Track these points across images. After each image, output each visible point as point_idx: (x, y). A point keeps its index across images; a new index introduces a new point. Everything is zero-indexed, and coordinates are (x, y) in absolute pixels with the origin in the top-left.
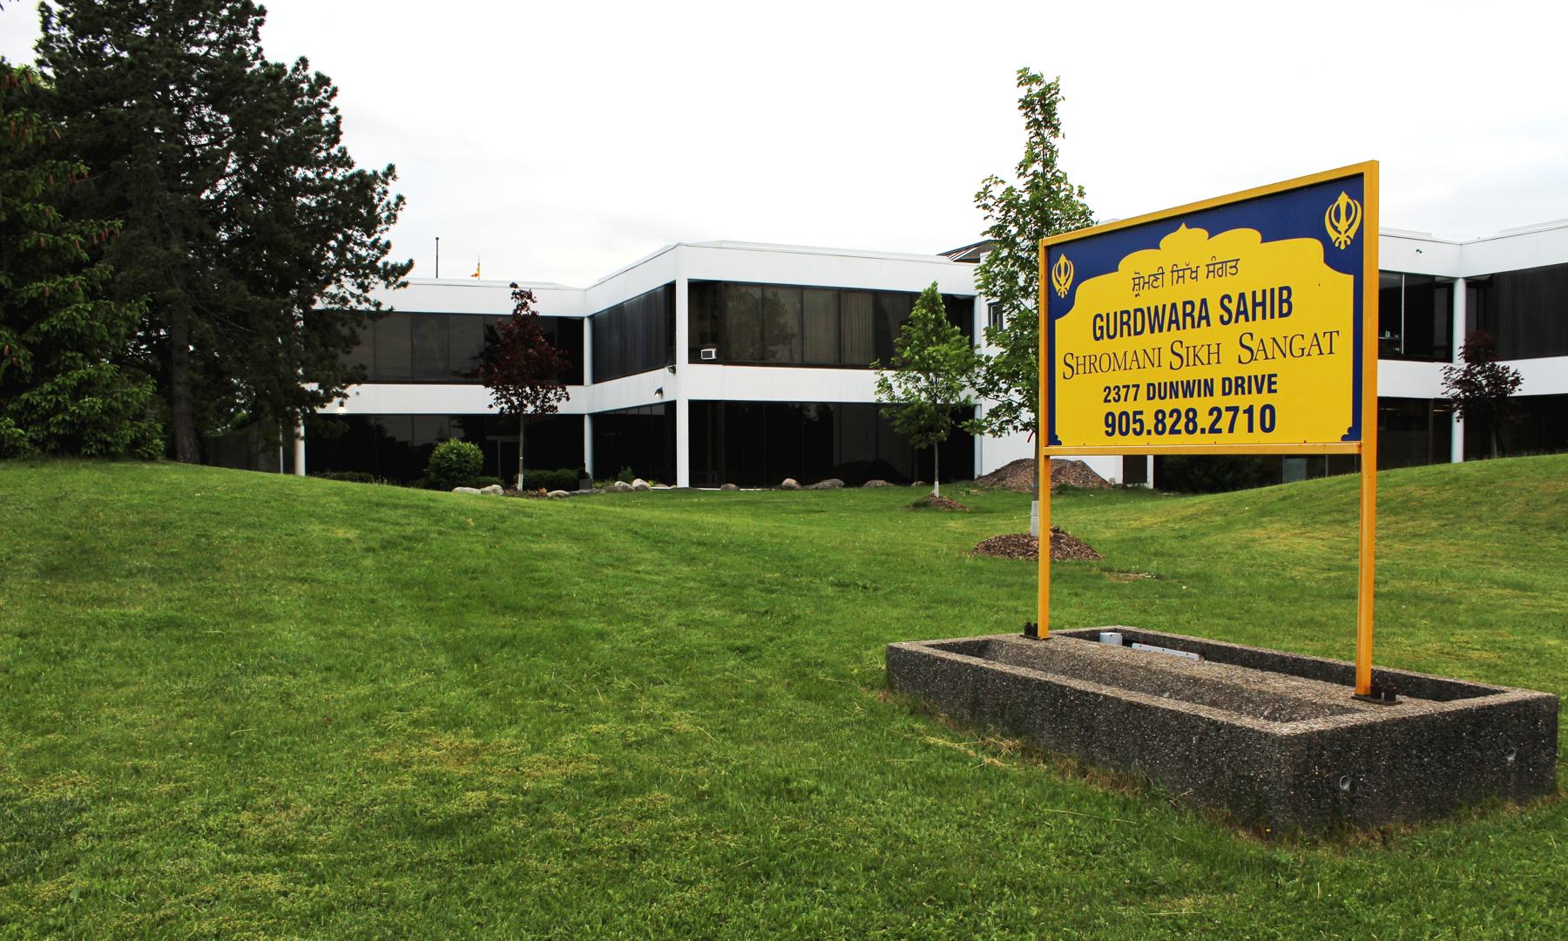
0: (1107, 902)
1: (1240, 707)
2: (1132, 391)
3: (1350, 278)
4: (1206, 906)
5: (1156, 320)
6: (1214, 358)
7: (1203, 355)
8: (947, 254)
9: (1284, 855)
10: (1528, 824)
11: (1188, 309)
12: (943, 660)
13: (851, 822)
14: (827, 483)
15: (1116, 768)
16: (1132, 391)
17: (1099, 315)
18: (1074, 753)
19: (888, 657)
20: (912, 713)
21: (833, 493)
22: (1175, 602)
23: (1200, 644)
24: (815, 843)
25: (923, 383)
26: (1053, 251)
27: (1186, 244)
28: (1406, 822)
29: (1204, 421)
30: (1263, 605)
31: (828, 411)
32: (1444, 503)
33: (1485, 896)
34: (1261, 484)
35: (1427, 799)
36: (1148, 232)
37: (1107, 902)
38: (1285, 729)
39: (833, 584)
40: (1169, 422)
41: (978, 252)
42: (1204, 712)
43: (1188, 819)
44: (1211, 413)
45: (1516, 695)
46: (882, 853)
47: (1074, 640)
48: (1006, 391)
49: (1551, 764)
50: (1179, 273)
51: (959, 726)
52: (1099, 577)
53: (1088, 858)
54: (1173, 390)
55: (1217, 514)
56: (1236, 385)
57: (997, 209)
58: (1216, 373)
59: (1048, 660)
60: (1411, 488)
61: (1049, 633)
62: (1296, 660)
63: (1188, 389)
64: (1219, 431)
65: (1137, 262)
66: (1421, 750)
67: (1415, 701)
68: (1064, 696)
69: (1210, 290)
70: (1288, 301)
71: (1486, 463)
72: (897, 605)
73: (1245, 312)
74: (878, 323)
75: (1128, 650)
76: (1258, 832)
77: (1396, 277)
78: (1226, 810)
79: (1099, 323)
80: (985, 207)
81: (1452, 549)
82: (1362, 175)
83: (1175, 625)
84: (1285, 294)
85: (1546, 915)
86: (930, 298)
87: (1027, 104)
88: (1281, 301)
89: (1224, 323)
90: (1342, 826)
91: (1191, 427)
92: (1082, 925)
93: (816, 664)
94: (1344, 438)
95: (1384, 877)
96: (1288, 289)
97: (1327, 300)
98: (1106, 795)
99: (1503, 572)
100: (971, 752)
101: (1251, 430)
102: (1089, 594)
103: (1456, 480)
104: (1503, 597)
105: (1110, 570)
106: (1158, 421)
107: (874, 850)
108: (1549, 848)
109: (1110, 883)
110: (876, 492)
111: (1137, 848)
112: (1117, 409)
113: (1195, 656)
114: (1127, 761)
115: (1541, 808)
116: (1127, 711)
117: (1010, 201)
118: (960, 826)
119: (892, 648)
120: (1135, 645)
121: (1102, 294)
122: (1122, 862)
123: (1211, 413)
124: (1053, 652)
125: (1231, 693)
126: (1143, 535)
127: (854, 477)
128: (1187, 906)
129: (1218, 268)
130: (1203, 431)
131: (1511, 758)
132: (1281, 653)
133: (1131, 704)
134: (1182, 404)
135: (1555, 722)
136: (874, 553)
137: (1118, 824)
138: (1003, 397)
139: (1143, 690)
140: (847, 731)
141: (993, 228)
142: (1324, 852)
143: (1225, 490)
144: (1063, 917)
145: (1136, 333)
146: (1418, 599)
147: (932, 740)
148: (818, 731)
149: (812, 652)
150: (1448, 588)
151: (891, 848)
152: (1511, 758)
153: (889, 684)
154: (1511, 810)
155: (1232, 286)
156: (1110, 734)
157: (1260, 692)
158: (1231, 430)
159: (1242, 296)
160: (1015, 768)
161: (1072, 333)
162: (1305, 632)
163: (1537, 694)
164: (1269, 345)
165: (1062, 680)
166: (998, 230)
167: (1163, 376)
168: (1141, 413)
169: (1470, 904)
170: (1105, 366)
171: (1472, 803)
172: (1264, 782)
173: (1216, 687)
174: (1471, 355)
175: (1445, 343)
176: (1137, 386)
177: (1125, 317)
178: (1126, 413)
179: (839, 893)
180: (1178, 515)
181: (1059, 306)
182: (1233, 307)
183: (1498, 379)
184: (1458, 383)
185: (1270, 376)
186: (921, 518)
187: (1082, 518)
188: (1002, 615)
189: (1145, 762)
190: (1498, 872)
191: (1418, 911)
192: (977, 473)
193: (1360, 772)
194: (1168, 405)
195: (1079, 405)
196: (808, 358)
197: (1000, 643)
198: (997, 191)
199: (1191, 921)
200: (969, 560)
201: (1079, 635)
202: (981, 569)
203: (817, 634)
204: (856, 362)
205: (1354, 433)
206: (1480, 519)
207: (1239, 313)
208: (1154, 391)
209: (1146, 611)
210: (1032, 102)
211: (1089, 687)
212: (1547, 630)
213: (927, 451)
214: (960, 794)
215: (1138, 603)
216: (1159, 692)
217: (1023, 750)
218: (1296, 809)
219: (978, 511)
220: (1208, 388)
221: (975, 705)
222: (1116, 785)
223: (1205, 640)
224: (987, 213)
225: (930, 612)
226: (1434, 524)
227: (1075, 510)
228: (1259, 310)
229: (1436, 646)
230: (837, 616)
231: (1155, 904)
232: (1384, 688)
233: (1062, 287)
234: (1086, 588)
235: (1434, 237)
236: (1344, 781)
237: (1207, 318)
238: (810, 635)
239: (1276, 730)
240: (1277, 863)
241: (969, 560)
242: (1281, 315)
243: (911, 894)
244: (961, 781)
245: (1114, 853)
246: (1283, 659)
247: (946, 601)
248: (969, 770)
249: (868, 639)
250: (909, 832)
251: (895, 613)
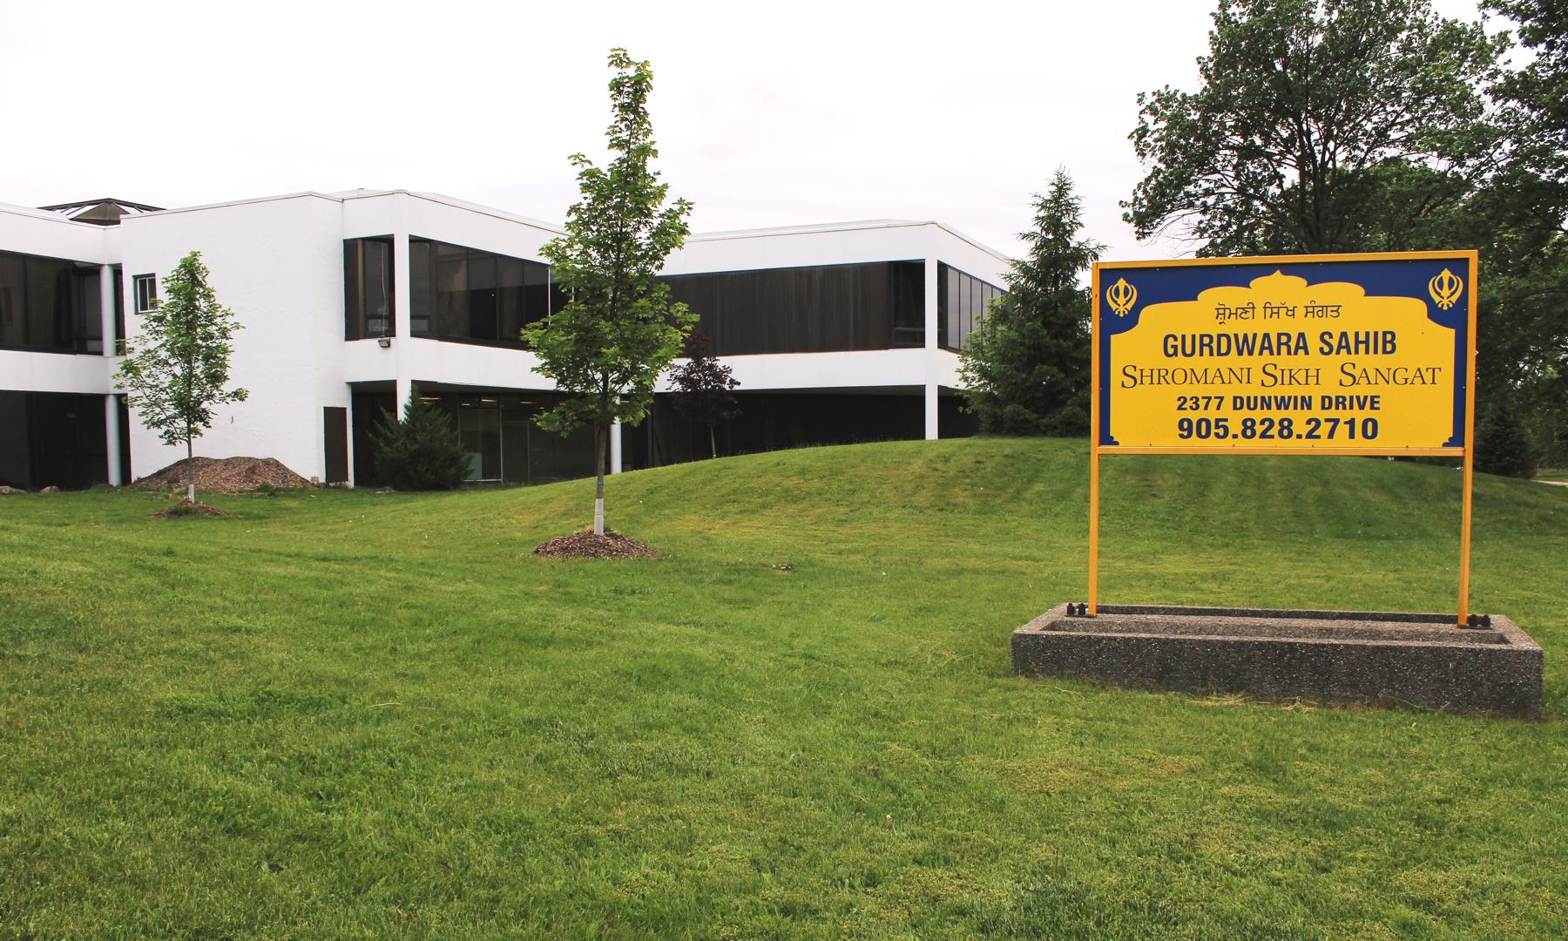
3: (1451, 333)
70: (1391, 342)
84: (1389, 337)
88: (1385, 342)
101: (1352, 436)
106: (1246, 428)
130: (1299, 437)
134: (1276, 415)
155: (1335, 327)
158: (1331, 436)
159: (1344, 335)
176: (1222, 398)
183: (719, 376)
205: (1457, 439)
207: (1340, 346)
208: (1238, 403)
220: (1307, 403)
242: (1385, 352)
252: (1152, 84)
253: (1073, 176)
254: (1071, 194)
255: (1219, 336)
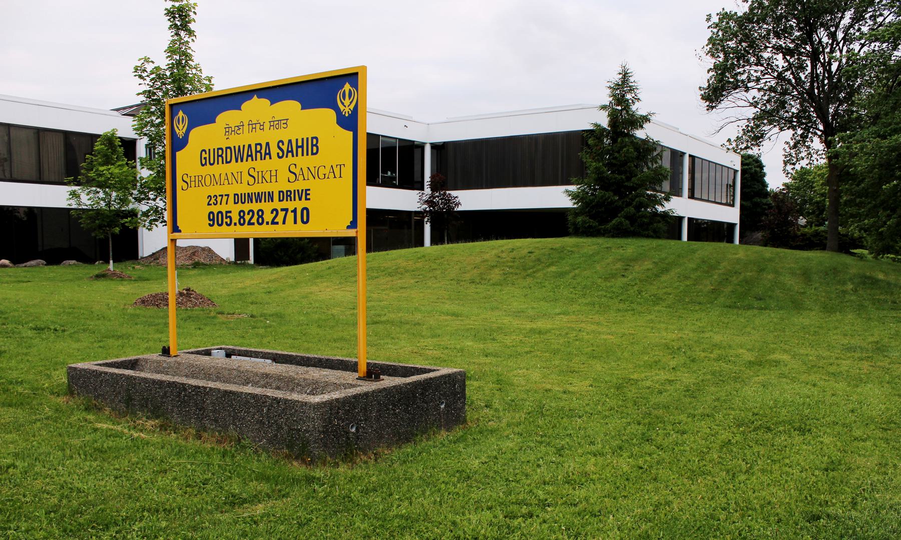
0: (210, 512)
1: (293, 389)
2: (225, 198)
3: (351, 133)
4: (272, 507)
5: (239, 154)
6: (274, 178)
7: (267, 177)
8: (117, 110)
9: (318, 473)
10: (450, 442)
11: (259, 148)
12: (106, 373)
13: (38, 484)
14: (33, 262)
15: (220, 432)
16: (225, 198)
17: (204, 150)
18: (193, 425)
19: (69, 374)
20: (86, 409)
21: (37, 269)
22: (261, 331)
23: (272, 354)
24: (9, 500)
25: (101, 195)
26: (174, 107)
27: (256, 107)
28: (388, 447)
29: (268, 217)
30: (314, 330)
31: (32, 212)
32: (418, 269)
33: (426, 482)
34: (317, 260)
35: (399, 433)
36: (235, 99)
37: (210, 512)
38: (316, 399)
39: (31, 329)
40: (247, 218)
41: (138, 110)
42: (270, 393)
43: (263, 458)
44: (272, 213)
45: (444, 371)
46: (60, 501)
47: (193, 356)
48: (154, 200)
49: (463, 407)
50: (253, 126)
51: (119, 415)
52: (214, 317)
53: (200, 487)
54: (249, 198)
55: (290, 278)
56: (286, 195)
57: (148, 79)
58: (274, 188)
59: (177, 369)
60: (400, 261)
61: (178, 353)
62: (327, 360)
63: (259, 198)
64: (277, 223)
65: (226, 118)
66: (394, 405)
67: (391, 378)
68: (185, 390)
69: (272, 137)
70: (316, 145)
71: (440, 247)
72: (78, 341)
73: (292, 151)
74: (71, 154)
75: (228, 360)
76: (304, 461)
77: (394, 141)
78: (286, 451)
79: (204, 155)
80: (141, 77)
81: (421, 295)
82: (357, 74)
83: (261, 344)
84: (315, 141)
85: (456, 488)
86: (109, 140)
87: (170, 13)
88: (313, 145)
89: (280, 158)
90: (352, 453)
91: (260, 221)
92: (195, 529)
93: (17, 382)
94: (348, 227)
95: (374, 479)
96: (316, 138)
97: (337, 146)
98: (213, 449)
99: (448, 307)
100: (126, 431)
101: (295, 222)
102: (208, 328)
103: (424, 256)
104: (446, 320)
105: (222, 313)
106: (241, 217)
107: (54, 500)
108: (460, 452)
109: (213, 501)
110: (70, 269)
111: (230, 478)
112: (215, 209)
113: (269, 361)
114: (225, 427)
115: (458, 432)
116: (224, 396)
117: (159, 76)
118: (116, 478)
119: (70, 368)
120: (233, 357)
121: (204, 137)
122: (221, 488)
123: (272, 213)
124: (179, 364)
125: (288, 381)
126: (244, 292)
127: (54, 258)
128: (260, 509)
129: (277, 124)
130: (267, 223)
131: (443, 406)
132: (320, 356)
133: (226, 391)
134: (255, 206)
135: (464, 385)
136: (64, 307)
137: (219, 466)
138: (152, 203)
139: (235, 383)
140: (38, 424)
141: (144, 92)
142: (342, 469)
143: (296, 264)
144: (183, 525)
145: (227, 162)
146: (402, 323)
147: (99, 425)
148: (18, 427)
149: (15, 375)
150: (418, 317)
151: (67, 497)
152: (443, 406)
153: (70, 392)
154: (444, 433)
155: (285, 135)
156: (214, 411)
157: (305, 379)
158: (284, 223)
159: (290, 141)
160: (156, 438)
161: (187, 161)
162: (337, 345)
163: (455, 370)
164: (305, 171)
165: (184, 380)
166: (149, 94)
167: (243, 189)
168: (230, 212)
169: (419, 486)
170: (208, 183)
171: (423, 433)
172: (307, 431)
173: (279, 378)
174: (434, 188)
175: (420, 180)
176: (228, 195)
177: (220, 152)
178: (221, 212)
179: (27, 531)
180: (267, 279)
181: (179, 144)
182: (285, 148)
183: (448, 201)
184: (427, 202)
185: (306, 190)
186: (101, 285)
187: (207, 282)
188: (151, 344)
189: (237, 427)
190: (434, 468)
191: (391, 495)
192: (140, 255)
193: (361, 421)
194: (247, 207)
195: (192, 205)
196: (15, 176)
197: (146, 361)
198: (149, 67)
199: (262, 517)
200: (130, 310)
201: (198, 353)
202: (138, 316)
203: (18, 363)
204: (53, 179)
205: (353, 224)
206: (436, 278)
207: (288, 152)
208: (238, 199)
209: (243, 337)
210: (173, 13)
211: (201, 383)
212: (467, 337)
213: (105, 241)
214: (117, 457)
215: (239, 332)
216: (246, 383)
217: (161, 426)
218: (325, 445)
219: (141, 279)
220: (271, 197)
221: (129, 401)
222: (219, 442)
223: (275, 351)
224: (141, 81)
225: (101, 344)
226: (412, 281)
227: (204, 278)
228: (300, 150)
229: (410, 349)
230: (34, 350)
231: (240, 511)
232: (374, 372)
233: (180, 131)
234: (205, 325)
235: (414, 119)
236: (352, 427)
237: (269, 154)
238: (13, 363)
239: (312, 400)
240: (314, 478)
241: (130, 310)
242: (313, 154)
243: (80, 524)
244: (118, 449)
245: (217, 483)
246: (320, 360)
247: (113, 336)
248: (122, 443)
249: (56, 364)
250: (80, 485)
251: (76, 345)
252: (715, 10)
253: (631, 68)
254: (632, 79)
255: (227, 148)
